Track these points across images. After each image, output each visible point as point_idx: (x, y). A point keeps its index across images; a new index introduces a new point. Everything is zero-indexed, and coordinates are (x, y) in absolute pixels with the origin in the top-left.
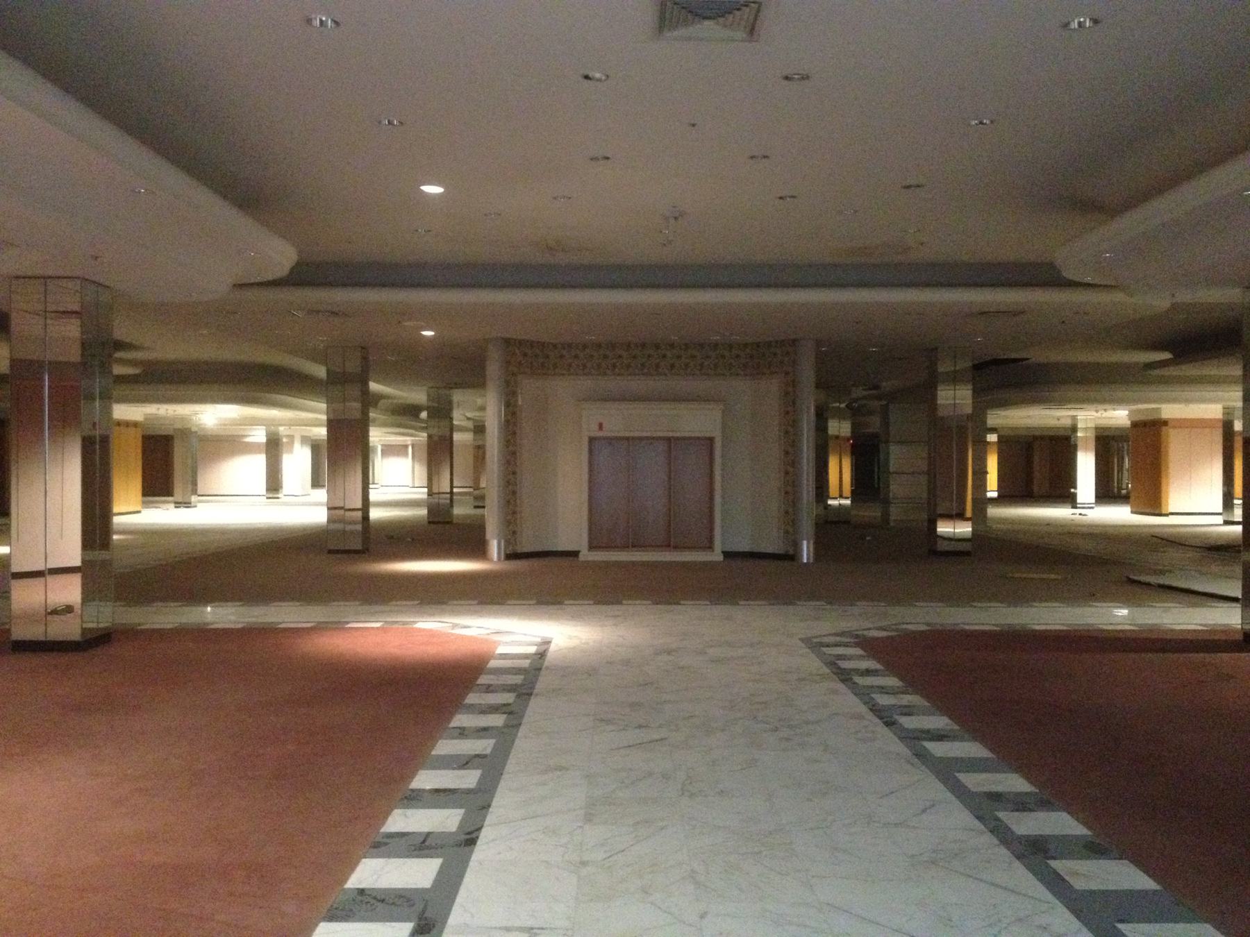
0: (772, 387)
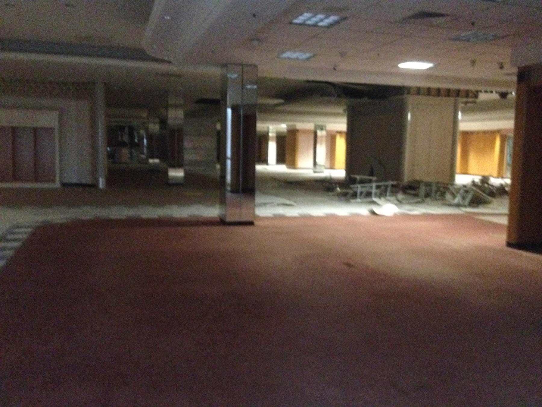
0: (84, 105)
